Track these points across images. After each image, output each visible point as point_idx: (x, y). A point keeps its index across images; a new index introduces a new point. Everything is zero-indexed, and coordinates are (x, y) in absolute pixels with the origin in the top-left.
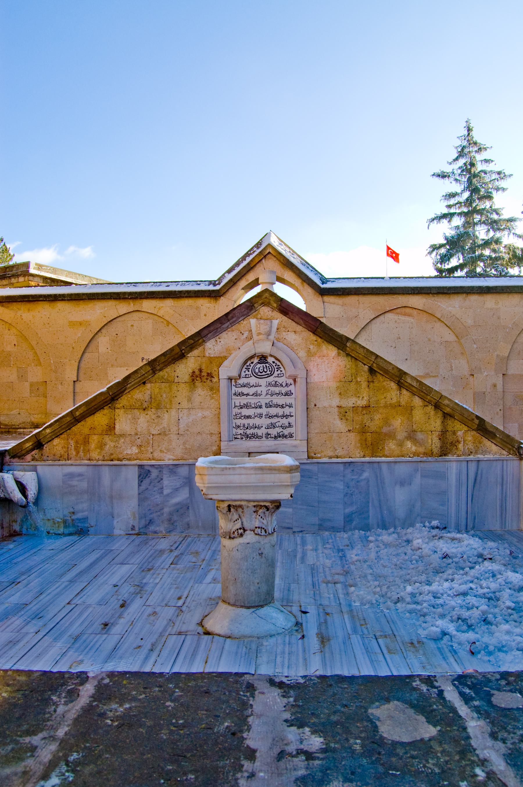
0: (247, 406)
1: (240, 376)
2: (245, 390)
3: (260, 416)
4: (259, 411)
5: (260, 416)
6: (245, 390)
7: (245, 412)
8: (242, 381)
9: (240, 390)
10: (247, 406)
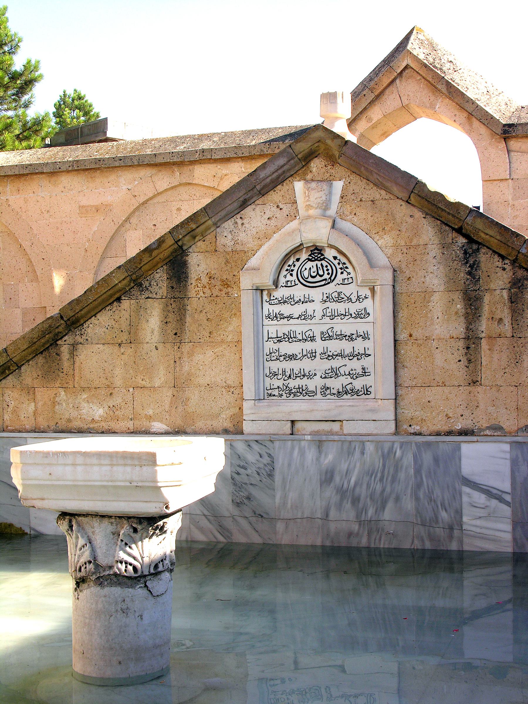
0: (289, 338)
1: (276, 283)
2: (286, 309)
3: (312, 355)
4: (309, 346)
5: (312, 355)
6: (286, 309)
7: (286, 348)
8: (281, 293)
9: (277, 309)
10: (289, 338)
